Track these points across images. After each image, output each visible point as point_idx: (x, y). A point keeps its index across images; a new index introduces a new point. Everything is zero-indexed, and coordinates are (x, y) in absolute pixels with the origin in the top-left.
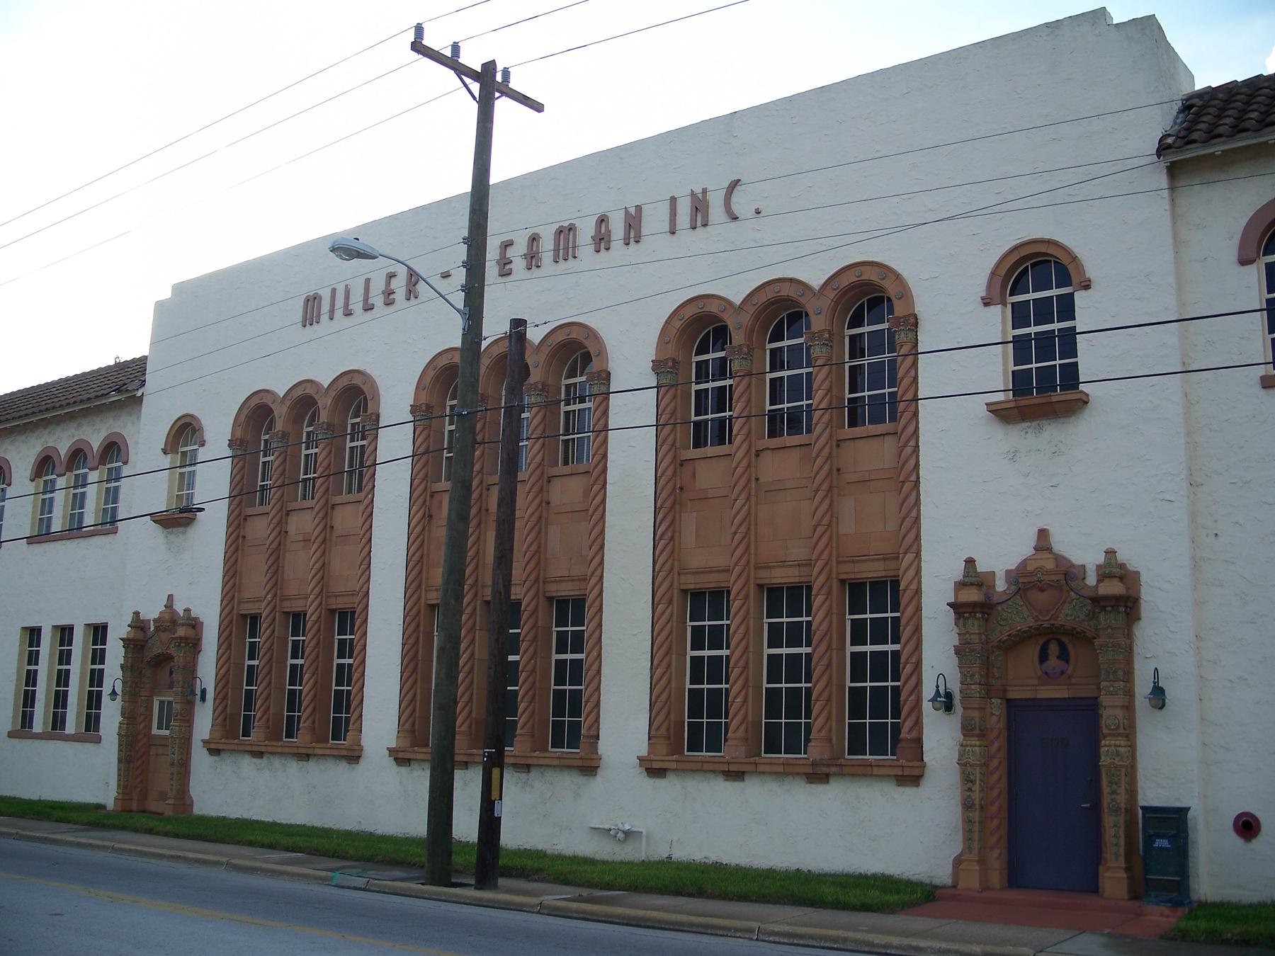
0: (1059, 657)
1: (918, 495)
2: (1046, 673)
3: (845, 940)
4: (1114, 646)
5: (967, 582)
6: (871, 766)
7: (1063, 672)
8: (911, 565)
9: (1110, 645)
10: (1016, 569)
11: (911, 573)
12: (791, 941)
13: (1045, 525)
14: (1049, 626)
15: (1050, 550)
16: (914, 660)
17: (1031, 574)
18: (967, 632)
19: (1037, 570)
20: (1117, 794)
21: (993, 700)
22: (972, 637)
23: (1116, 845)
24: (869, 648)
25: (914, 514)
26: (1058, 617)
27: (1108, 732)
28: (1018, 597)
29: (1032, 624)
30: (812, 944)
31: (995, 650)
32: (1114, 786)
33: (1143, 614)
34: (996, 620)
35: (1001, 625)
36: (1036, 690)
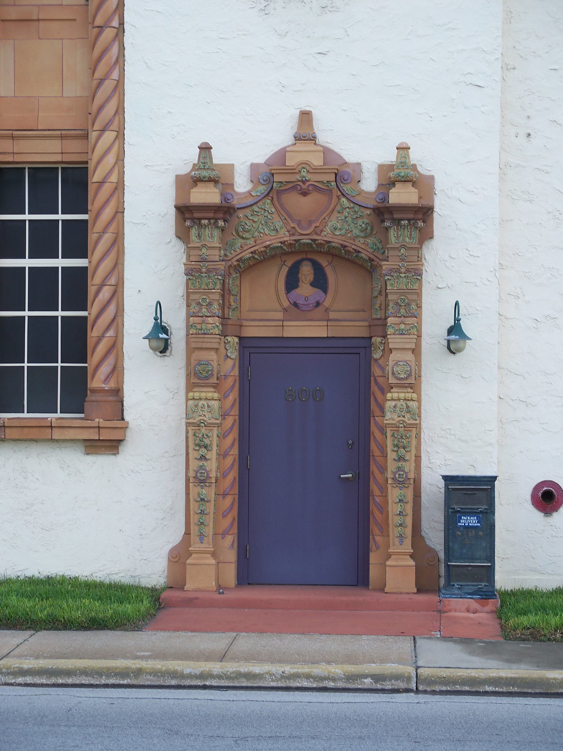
0: (313, 284)
1: (122, 48)
2: (296, 305)
3: (139, 672)
4: (408, 271)
5: (204, 177)
6: (51, 427)
7: (318, 304)
8: (109, 150)
9: (403, 270)
10: (265, 163)
11: (111, 159)
12: (53, 680)
13: (306, 106)
14: (310, 241)
15: (313, 139)
16: (113, 281)
17: (292, 171)
18: (204, 246)
20: (405, 461)
21: (229, 338)
22: (209, 252)
23: (401, 525)
24: (60, 263)
25: (115, 75)
26: (322, 231)
28: (268, 201)
29: (286, 239)
30: (87, 682)
31: (232, 272)
33: (436, 233)
34: (237, 231)
35: (243, 238)
36: (241, 326)
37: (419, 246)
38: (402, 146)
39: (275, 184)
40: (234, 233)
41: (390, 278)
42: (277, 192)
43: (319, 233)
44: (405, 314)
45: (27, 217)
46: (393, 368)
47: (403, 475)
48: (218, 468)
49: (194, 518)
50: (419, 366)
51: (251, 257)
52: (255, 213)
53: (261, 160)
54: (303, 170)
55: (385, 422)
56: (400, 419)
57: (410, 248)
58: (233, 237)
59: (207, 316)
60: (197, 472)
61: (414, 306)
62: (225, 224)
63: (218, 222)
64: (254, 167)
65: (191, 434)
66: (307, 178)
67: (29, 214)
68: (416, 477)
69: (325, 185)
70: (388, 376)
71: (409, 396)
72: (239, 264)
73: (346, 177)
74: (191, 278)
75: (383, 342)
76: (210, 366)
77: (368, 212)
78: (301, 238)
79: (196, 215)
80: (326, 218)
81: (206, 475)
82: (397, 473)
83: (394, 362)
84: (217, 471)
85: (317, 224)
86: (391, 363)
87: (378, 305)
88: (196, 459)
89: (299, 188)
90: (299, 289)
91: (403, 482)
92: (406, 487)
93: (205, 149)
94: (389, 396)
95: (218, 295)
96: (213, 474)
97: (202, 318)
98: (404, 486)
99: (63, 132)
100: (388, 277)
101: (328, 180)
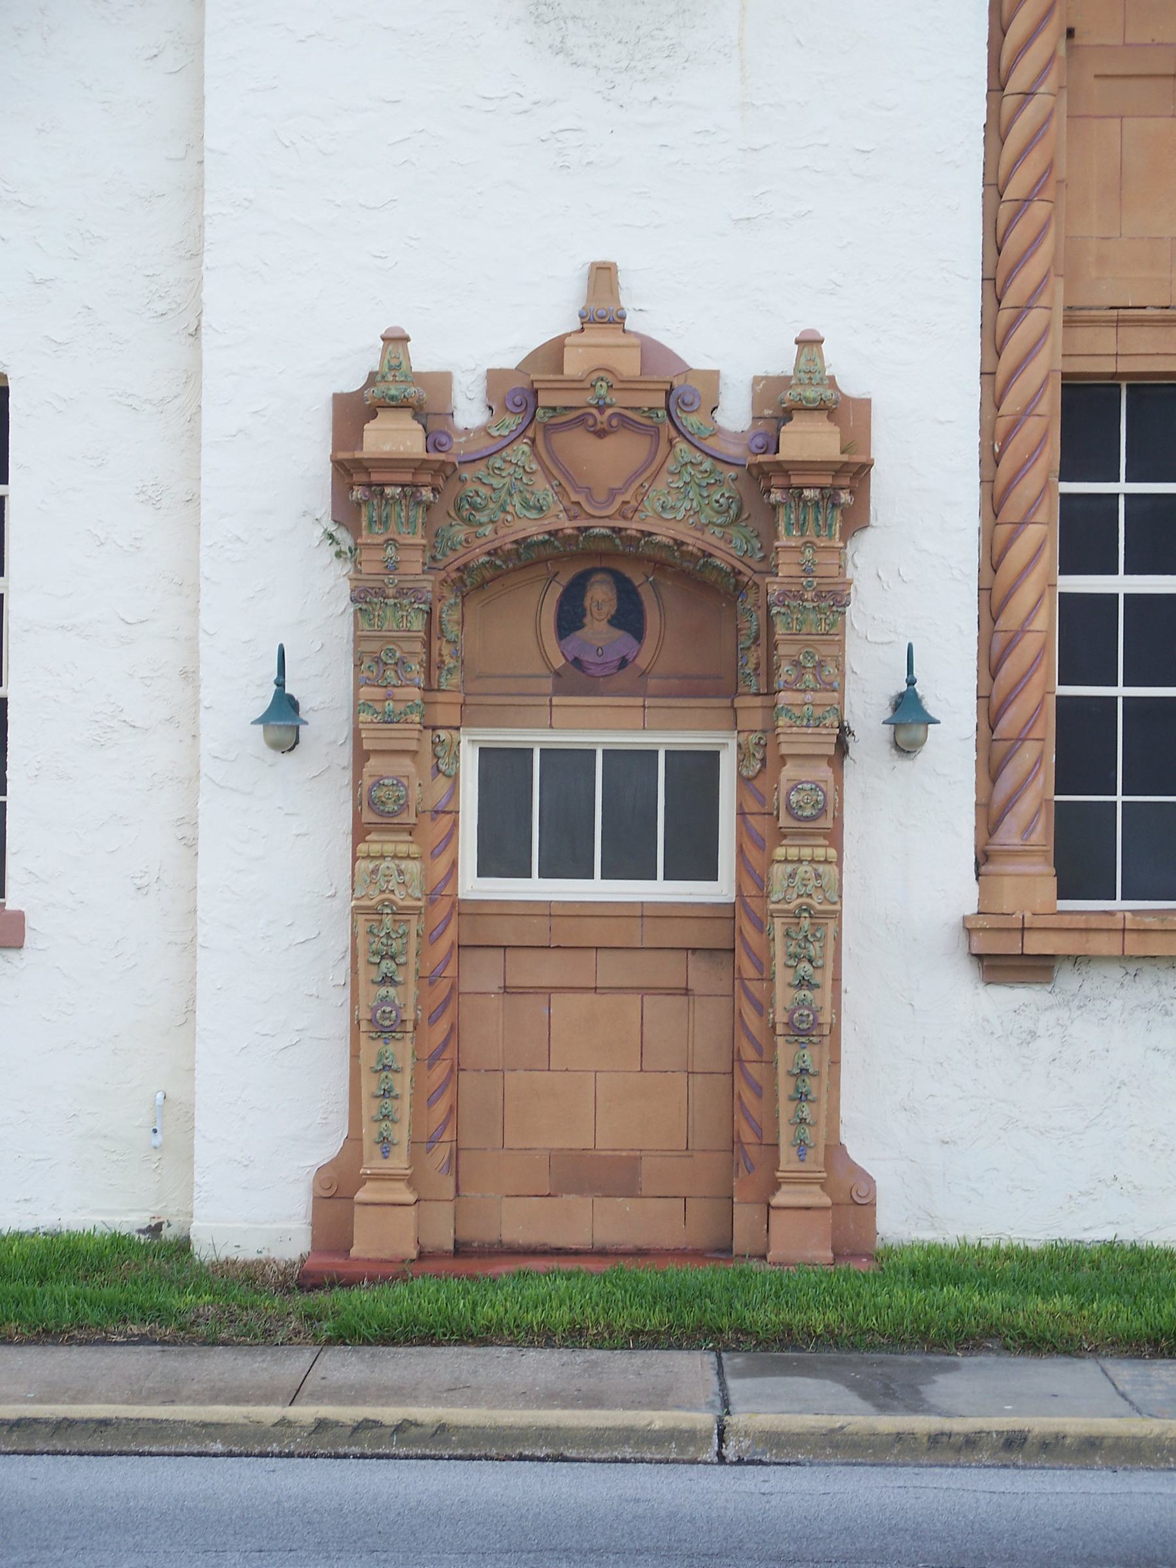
2: (577, 662)
4: (819, 596)
7: (623, 663)
9: (391, 592)
19: (595, 376)
27: (373, 818)
28: (526, 448)
32: (805, 966)
37: (841, 545)
38: (391, 335)
39: (540, 412)
40: (453, 514)
41: (783, 610)
42: (545, 426)
43: (630, 515)
44: (394, 682)
45: (1122, 487)
46: (788, 794)
47: (808, 1015)
48: (418, 1000)
49: (370, 1108)
50: (840, 792)
51: (488, 562)
52: (496, 471)
53: (510, 361)
54: (599, 384)
55: (772, 907)
56: (384, 896)
57: (404, 545)
58: (450, 520)
59: (394, 686)
60: (374, 1010)
61: (831, 669)
62: (435, 496)
63: (839, 495)
64: (494, 377)
65: (362, 929)
66: (608, 401)
67: (1127, 480)
68: (834, 1021)
69: (645, 415)
70: (778, 813)
71: (820, 853)
72: (461, 579)
73: (688, 399)
74: (364, 607)
75: (762, 742)
76: (402, 788)
77: (732, 473)
78: (591, 525)
79: (376, 477)
80: (645, 484)
81: (811, 1017)
82: (809, 1010)
83: (792, 784)
84: (416, 1009)
85: (627, 497)
86: (784, 787)
87: (751, 665)
88: (790, 985)
89: (591, 422)
90: (585, 630)
91: (392, 1029)
92: (398, 1039)
93: (396, 340)
94: (780, 852)
95: (420, 644)
96: (409, 1015)
97: (383, 690)
98: (811, 1041)
99: (1121, 312)
100: (779, 609)
101: (652, 406)
